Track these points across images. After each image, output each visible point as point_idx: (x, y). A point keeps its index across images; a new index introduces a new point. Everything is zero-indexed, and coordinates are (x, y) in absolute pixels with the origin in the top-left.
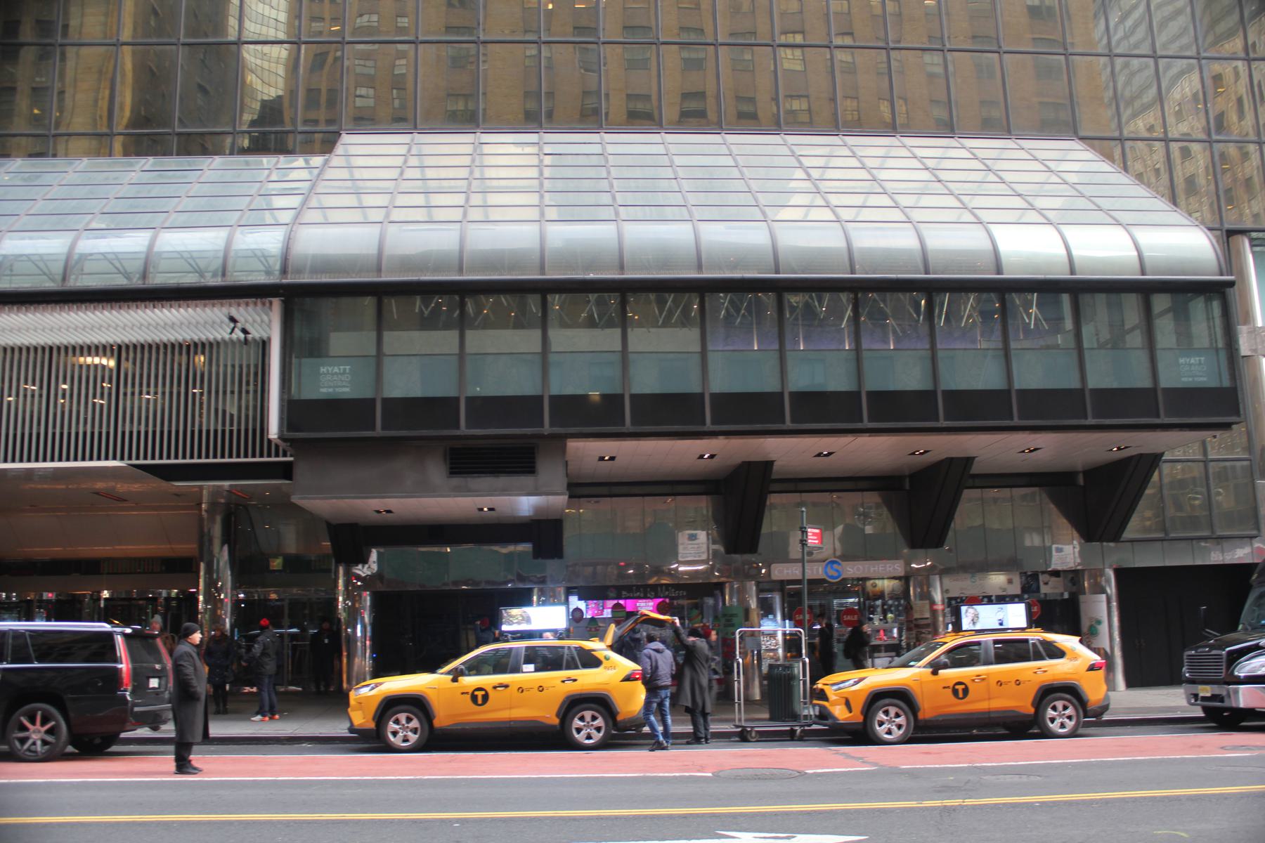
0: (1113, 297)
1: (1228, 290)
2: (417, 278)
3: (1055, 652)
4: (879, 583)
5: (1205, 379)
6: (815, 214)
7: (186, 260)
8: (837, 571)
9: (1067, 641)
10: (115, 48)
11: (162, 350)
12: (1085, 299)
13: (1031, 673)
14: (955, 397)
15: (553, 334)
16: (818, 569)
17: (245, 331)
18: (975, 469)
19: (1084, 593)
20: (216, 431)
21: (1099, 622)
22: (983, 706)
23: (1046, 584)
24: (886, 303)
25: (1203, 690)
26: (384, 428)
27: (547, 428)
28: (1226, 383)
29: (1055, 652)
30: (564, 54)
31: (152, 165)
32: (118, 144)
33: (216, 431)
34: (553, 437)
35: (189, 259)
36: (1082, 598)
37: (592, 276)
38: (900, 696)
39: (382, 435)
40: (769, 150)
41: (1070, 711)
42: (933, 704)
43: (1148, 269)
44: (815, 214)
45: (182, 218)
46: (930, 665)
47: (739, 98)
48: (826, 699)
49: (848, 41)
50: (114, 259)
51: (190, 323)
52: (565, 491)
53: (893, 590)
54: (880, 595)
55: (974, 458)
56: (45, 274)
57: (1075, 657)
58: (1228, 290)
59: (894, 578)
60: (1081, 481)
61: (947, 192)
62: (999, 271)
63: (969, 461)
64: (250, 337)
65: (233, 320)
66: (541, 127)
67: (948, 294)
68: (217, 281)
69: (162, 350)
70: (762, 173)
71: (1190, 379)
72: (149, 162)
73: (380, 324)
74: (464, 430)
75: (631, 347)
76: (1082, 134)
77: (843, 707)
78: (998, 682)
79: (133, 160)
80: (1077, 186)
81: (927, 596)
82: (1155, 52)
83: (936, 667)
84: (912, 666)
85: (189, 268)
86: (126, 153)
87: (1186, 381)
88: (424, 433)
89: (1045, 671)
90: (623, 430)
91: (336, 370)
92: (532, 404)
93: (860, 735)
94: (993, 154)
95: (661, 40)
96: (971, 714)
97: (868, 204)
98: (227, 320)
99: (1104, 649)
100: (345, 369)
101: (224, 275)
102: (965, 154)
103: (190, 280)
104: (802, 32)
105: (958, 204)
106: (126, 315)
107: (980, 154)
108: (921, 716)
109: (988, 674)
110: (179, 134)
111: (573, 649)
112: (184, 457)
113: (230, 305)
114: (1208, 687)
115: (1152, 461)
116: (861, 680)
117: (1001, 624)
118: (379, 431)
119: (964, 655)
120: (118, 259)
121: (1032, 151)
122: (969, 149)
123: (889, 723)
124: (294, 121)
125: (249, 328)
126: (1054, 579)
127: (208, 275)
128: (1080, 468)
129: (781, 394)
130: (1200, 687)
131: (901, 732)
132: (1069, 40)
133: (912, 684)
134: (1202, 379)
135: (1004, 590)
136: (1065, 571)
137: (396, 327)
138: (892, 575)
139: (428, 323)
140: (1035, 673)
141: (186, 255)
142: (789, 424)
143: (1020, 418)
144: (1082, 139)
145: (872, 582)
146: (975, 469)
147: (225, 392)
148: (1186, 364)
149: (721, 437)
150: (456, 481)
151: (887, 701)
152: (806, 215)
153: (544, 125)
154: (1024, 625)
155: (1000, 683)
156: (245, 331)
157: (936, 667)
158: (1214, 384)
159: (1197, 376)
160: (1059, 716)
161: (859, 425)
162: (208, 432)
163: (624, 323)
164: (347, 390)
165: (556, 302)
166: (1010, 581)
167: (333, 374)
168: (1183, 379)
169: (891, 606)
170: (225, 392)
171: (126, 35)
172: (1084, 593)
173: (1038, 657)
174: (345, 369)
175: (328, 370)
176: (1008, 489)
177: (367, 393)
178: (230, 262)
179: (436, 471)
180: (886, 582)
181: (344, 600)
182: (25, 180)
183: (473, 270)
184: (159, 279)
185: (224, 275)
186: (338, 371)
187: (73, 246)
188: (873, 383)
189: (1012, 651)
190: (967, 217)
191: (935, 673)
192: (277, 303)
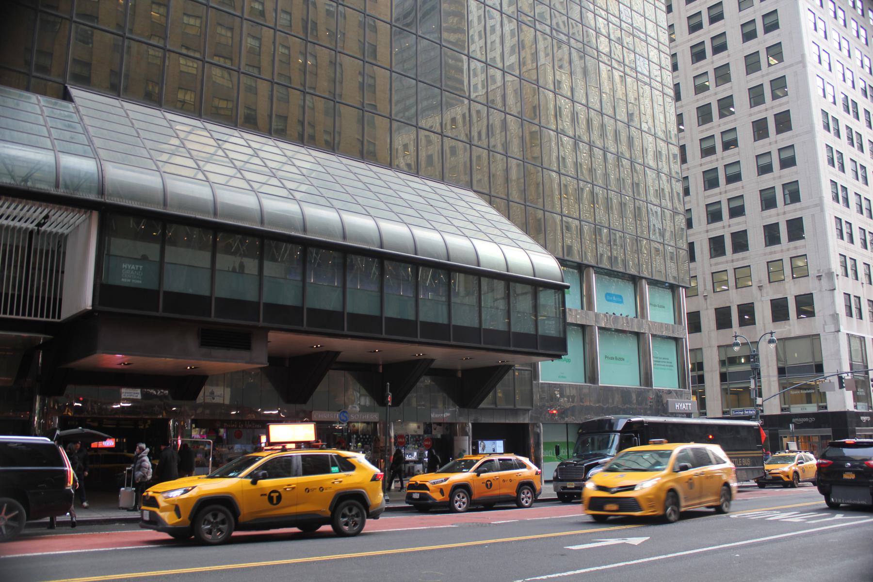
1: (566, 290)
2: (194, 216)
3: (523, 466)
4: (356, 425)
5: (140, 282)
6: (234, 182)
8: (346, 417)
9: (525, 460)
12: (351, 258)
13: (515, 476)
14: (315, 313)
15: (220, 257)
16: (336, 416)
18: (340, 358)
19: (457, 435)
21: (464, 451)
22: (497, 492)
23: (435, 429)
24: (359, 261)
25: (569, 484)
27: (261, 323)
28: (562, 336)
29: (523, 466)
30: (320, 104)
34: (262, 328)
36: (455, 438)
37: (293, 233)
38: (463, 487)
40: (109, 109)
41: (529, 495)
42: (478, 492)
43: (419, 252)
44: (234, 182)
46: (250, 475)
47: (249, 108)
48: (428, 489)
49: (312, 91)
50: (15, 158)
52: (267, 362)
53: (363, 429)
54: (356, 432)
55: (435, 360)
57: (530, 468)
58: (566, 290)
59: (364, 422)
60: (460, 375)
61: (189, 156)
62: (479, 265)
63: (337, 353)
66: (119, 96)
67: (285, 244)
70: (154, 136)
71: (129, 281)
73: (163, 241)
74: (213, 318)
75: (167, 259)
76: (475, 188)
77: (439, 494)
78: (306, 489)
80: (272, 170)
81: (386, 433)
82: (391, 115)
83: (254, 478)
84: (464, 472)
89: (341, 482)
90: (302, 329)
91: (133, 267)
92: (255, 306)
93: (447, 508)
94: (141, 117)
95: (127, 35)
96: (500, 495)
97: (268, 183)
99: (559, 466)
100: (139, 268)
102: (242, 142)
104: (231, 60)
105: (195, 166)
107: (253, 145)
108: (473, 498)
109: (297, 484)
111: (334, 458)
112: (54, 317)
114: (573, 483)
115: (507, 368)
116: (446, 480)
117: (494, 451)
118: (161, 313)
119: (488, 466)
121: (248, 141)
122: (314, 157)
123: (460, 502)
126: (438, 427)
129: (210, 298)
130: (568, 483)
131: (465, 506)
132: (337, 92)
133: (469, 480)
134: (138, 282)
135: (416, 432)
136: (444, 423)
137: (174, 243)
138: (364, 421)
139: (145, 237)
140: (333, 483)
142: (305, 327)
143: (386, 333)
144: (475, 191)
145: (352, 424)
146: (340, 358)
148: (127, 269)
149: (349, 339)
150: (204, 350)
151: (459, 490)
152: (228, 181)
153: (203, 117)
154: (503, 452)
155: (504, 481)
157: (254, 478)
160: (526, 497)
163: (163, 241)
165: (389, 266)
166: (419, 427)
167: (131, 270)
169: (361, 439)
172: (457, 435)
173: (517, 468)
174: (139, 268)
175: (127, 267)
176: (343, 372)
177: (152, 285)
179: (192, 342)
180: (360, 424)
181: (39, 419)
182: (65, 126)
186: (134, 268)
188: (267, 298)
189: (506, 465)
190: (200, 176)
191: (254, 483)
192: (95, 215)
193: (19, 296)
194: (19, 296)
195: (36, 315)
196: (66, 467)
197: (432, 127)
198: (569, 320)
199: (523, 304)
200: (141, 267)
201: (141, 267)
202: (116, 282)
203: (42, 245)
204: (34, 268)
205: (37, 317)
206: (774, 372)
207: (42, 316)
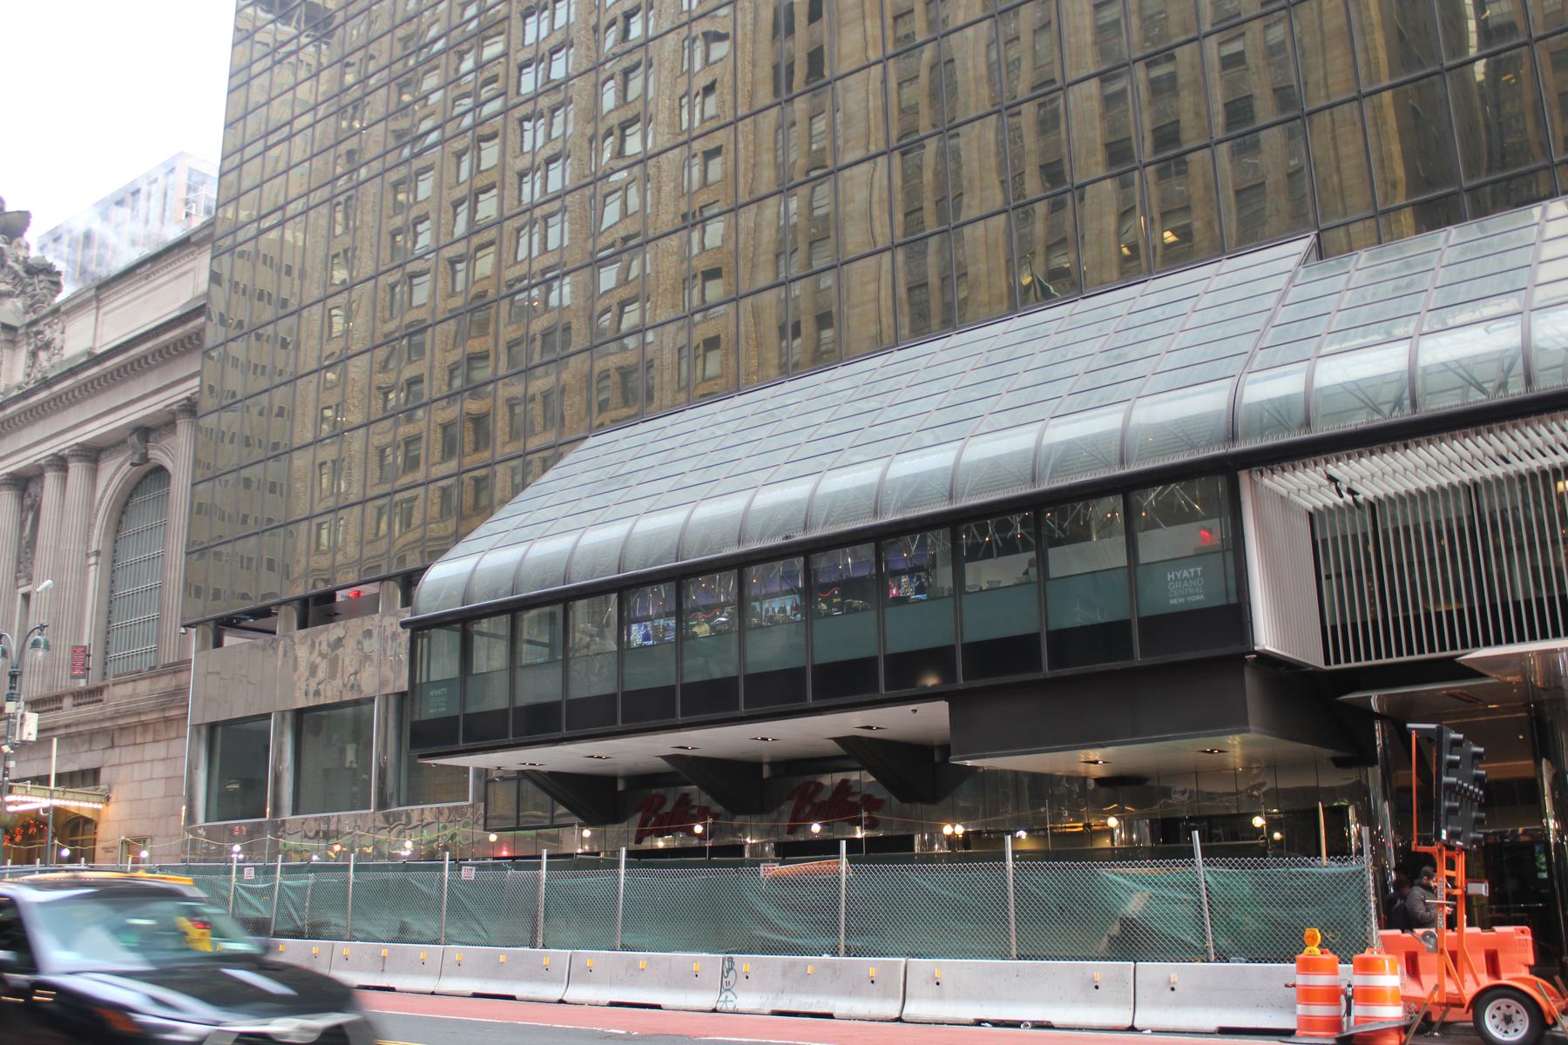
0: (596, 600)
7: (1455, 373)
10: (1207, 152)
11: (1483, 492)
17: (1351, 492)
20: (1539, 601)
26: (1051, 667)
28: (1233, 600)
31: (1303, 277)
32: (1407, 218)
33: (1539, 601)
35: (1359, 392)
39: (1049, 676)
45: (1004, 419)
51: (1373, 475)
56: (1367, 405)
64: (1360, 498)
65: (1332, 479)
68: (1405, 415)
69: (1518, 487)
71: (1182, 600)
72: (1453, 233)
79: (1428, 235)
85: (1358, 404)
86: (1418, 231)
87: (1176, 602)
88: (1181, 657)
90: (879, 697)
91: (1186, 574)
98: (1326, 482)
100: (1196, 572)
101: (1414, 404)
103: (1360, 421)
106: (1518, 435)
110: (1470, 190)
113: (1327, 462)
120: (1461, 366)
124: (1545, 148)
125: (1356, 487)
127: (1386, 409)
128: (621, 771)
134: (1198, 598)
141: (1453, 366)
147: (1339, 575)
156: (1351, 492)
158: (1220, 601)
159: (1189, 595)
161: (613, 728)
162: (1528, 602)
164: (444, 709)
167: (1182, 580)
168: (1172, 602)
170: (1339, 575)
171: (1219, 134)
178: (1312, 406)
183: (974, 492)
184: (1322, 430)
185: (1414, 404)
187: (689, 516)
193: (1471, 610)
194: (1471, 610)
195: (1368, 657)
196: (13, 863)
197: (1016, 14)
198: (1244, 477)
199: (445, 644)
200: (1199, 569)
201: (1199, 569)
202: (424, 718)
203: (1354, 527)
204: (1369, 570)
205: (1456, 648)
206: (1231, 193)
207: (1400, 653)
